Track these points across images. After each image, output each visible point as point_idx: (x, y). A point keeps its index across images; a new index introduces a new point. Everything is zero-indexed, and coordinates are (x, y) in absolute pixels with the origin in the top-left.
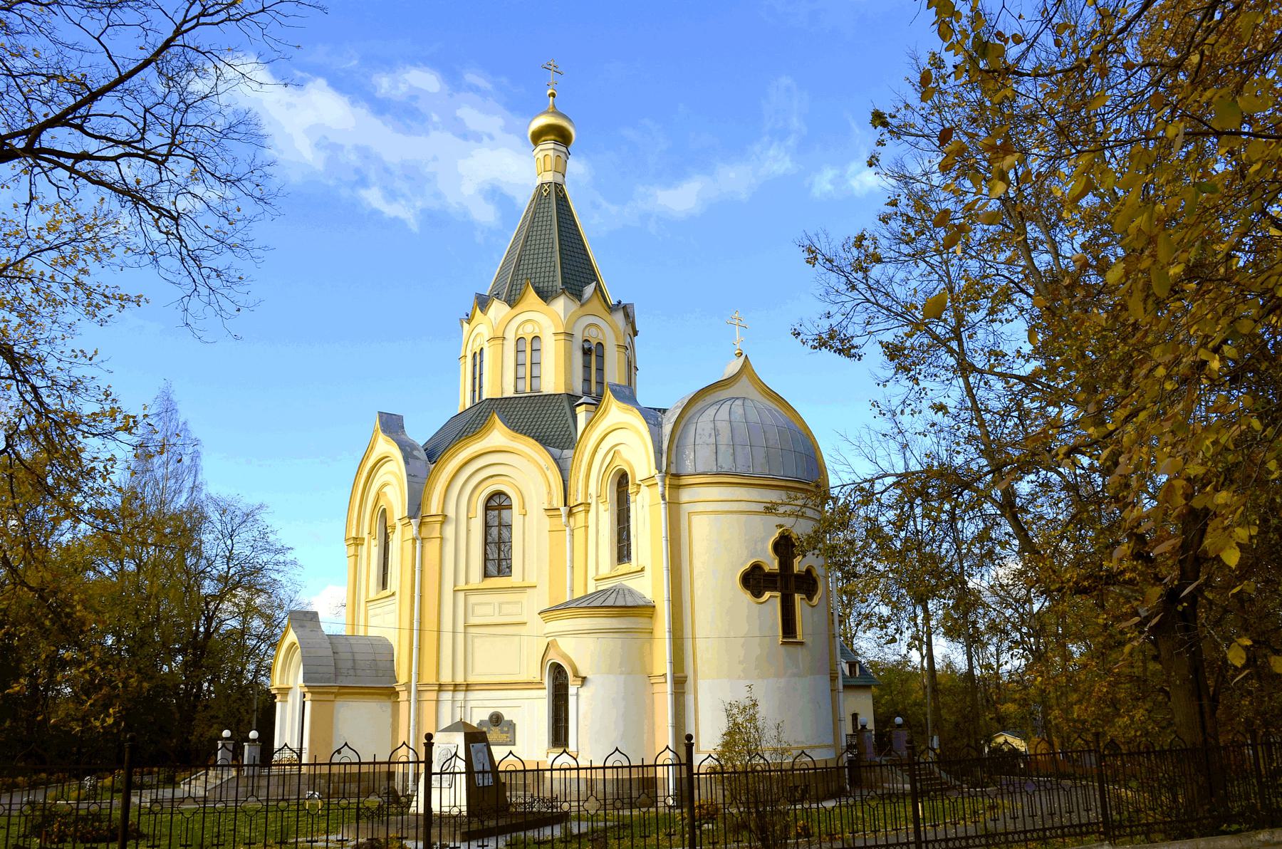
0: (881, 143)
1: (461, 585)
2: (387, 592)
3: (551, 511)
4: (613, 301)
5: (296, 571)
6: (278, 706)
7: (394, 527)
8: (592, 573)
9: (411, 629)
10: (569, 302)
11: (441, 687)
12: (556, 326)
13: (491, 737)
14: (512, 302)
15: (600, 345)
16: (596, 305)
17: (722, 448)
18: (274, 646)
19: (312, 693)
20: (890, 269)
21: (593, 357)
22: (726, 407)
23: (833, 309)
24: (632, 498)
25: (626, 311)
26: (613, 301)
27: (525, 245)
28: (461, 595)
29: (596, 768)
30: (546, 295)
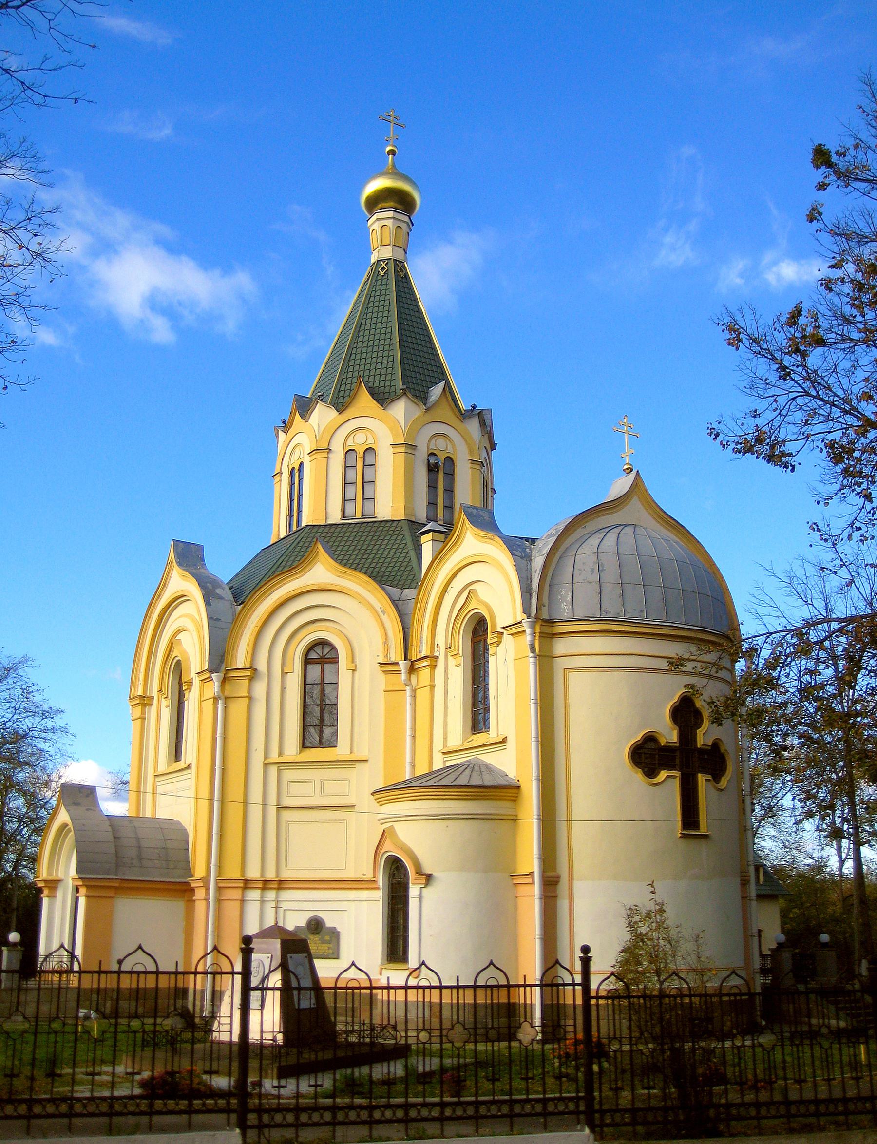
0: (822, 186)
1: (274, 756)
2: (181, 764)
3: (388, 666)
4: (464, 406)
5: (66, 739)
6: (45, 902)
7: (190, 683)
8: (438, 745)
9: (211, 800)
10: (412, 407)
11: (247, 884)
12: (395, 436)
13: (312, 947)
14: (340, 405)
15: (450, 460)
16: (445, 412)
17: (607, 588)
18: (38, 831)
19: (87, 886)
20: (833, 355)
21: (441, 476)
22: (611, 538)
23: (761, 405)
24: (492, 650)
25: (482, 418)
26: (464, 406)
27: (348, 360)
28: (273, 770)
29: (531, 986)
30: (383, 398)
